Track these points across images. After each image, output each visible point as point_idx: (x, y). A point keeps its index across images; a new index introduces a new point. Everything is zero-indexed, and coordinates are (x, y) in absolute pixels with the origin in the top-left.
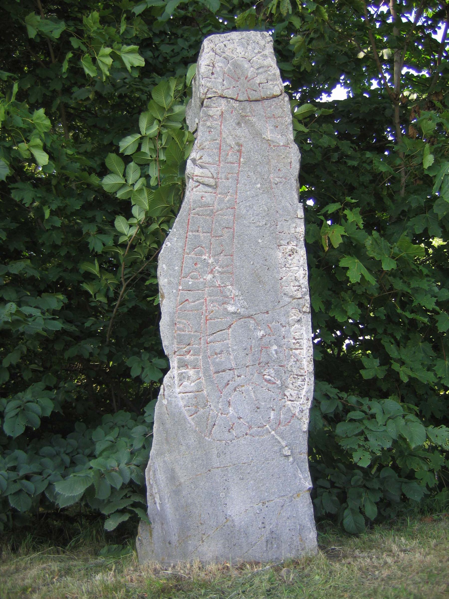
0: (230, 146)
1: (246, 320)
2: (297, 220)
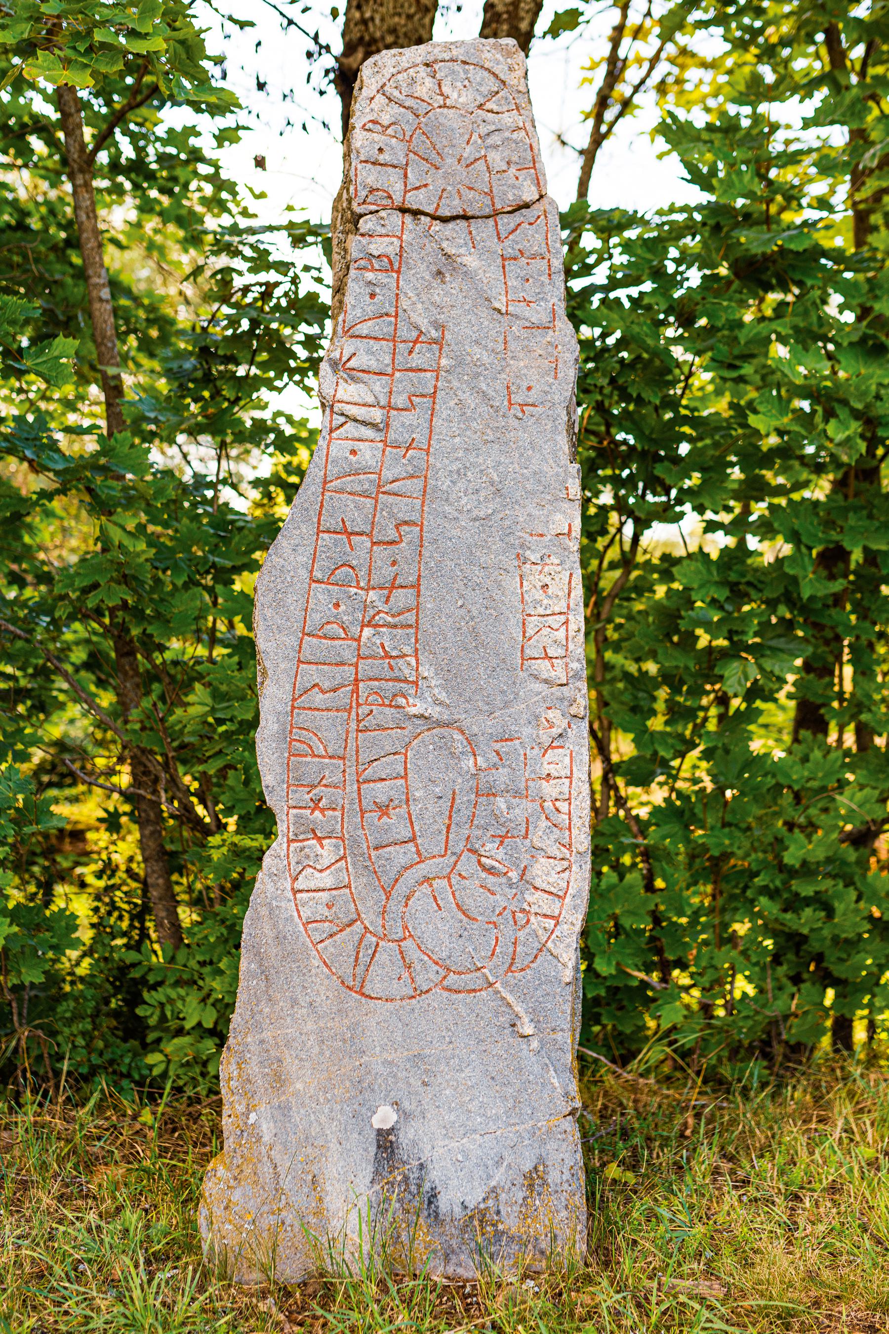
0: (417, 328)
1: (444, 731)
2: (566, 505)
